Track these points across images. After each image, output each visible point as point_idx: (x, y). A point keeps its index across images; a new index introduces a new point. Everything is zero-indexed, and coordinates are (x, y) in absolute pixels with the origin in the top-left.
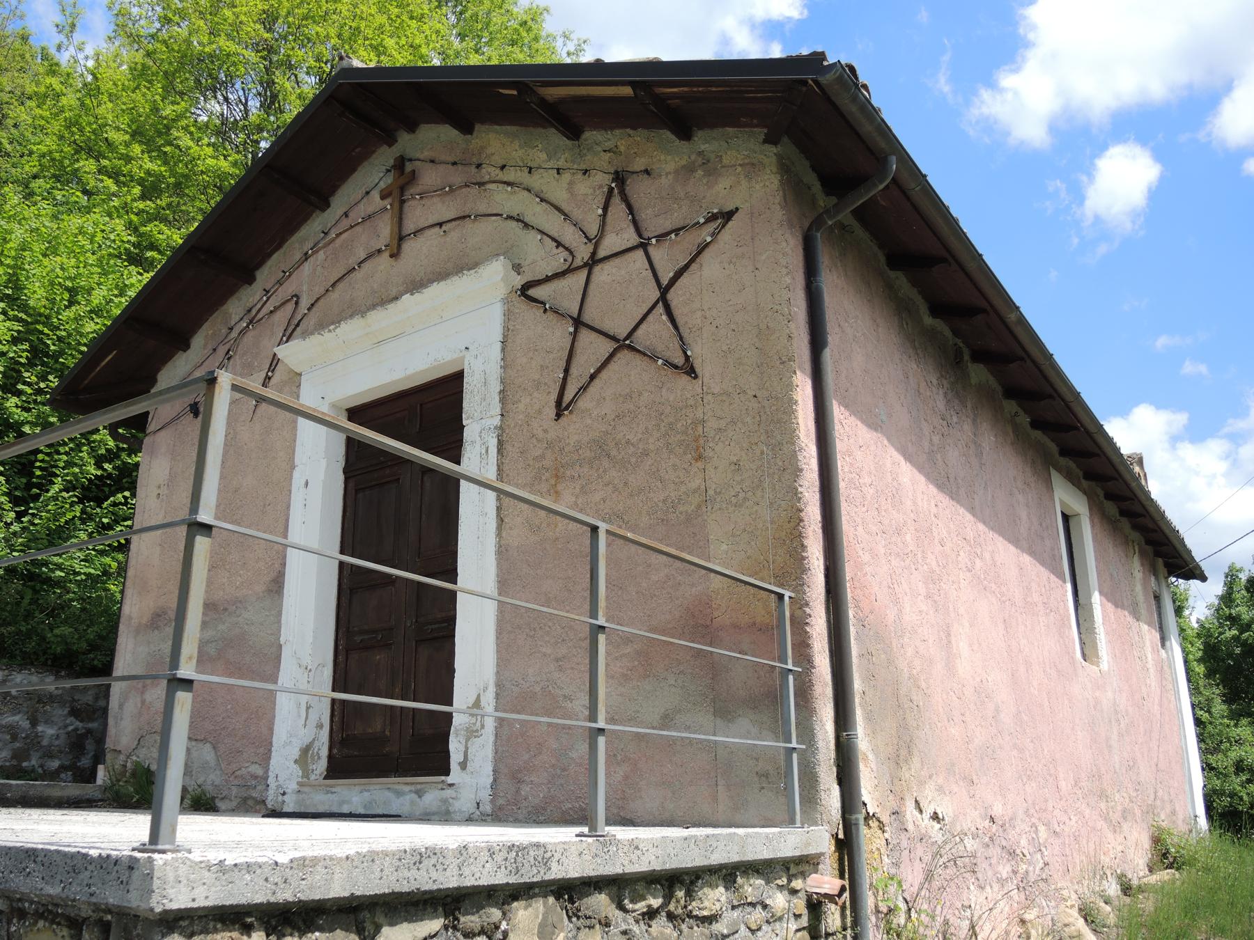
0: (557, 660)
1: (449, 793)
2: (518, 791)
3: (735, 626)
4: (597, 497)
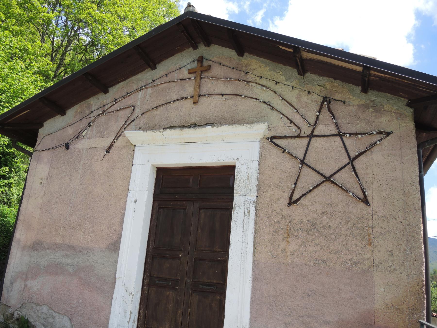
4: (311, 249)
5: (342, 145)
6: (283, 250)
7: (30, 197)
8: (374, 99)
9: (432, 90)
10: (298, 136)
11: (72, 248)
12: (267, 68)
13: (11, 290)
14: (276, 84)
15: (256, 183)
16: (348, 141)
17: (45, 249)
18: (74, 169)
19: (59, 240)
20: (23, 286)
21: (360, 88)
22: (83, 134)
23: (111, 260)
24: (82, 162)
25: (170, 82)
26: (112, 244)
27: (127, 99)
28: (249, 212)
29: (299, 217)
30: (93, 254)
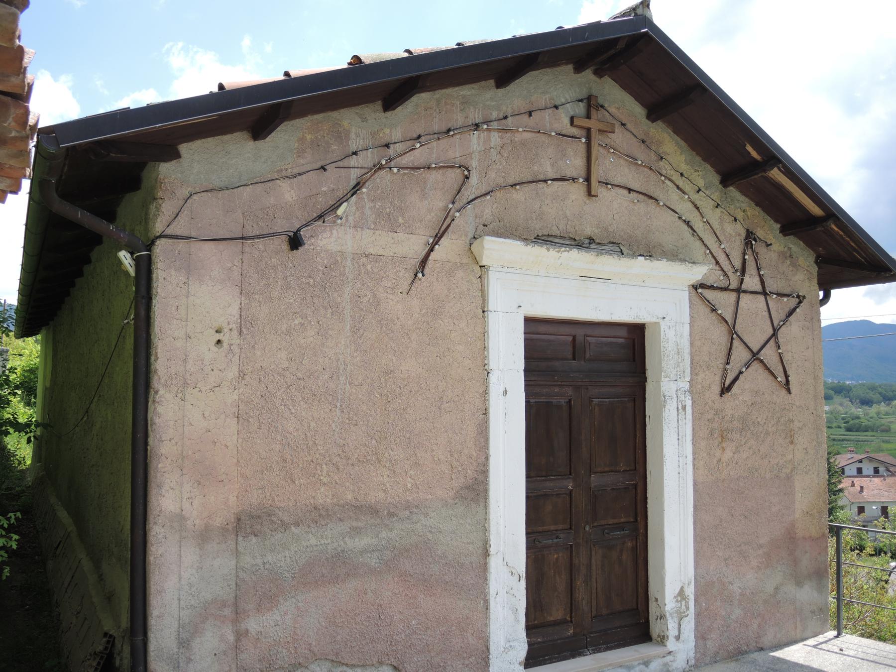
0: (726, 560)
1: (669, 658)
2: (706, 645)
3: (804, 538)
4: (744, 455)
5: (766, 308)
6: (719, 461)
7: (186, 384)
8: (791, 246)
9: (863, 258)
10: (726, 289)
11: (372, 510)
12: (683, 158)
13: (189, 660)
14: (698, 192)
15: (492, 318)
16: (773, 301)
17: (285, 526)
18: (326, 309)
19: (323, 497)
20: (231, 638)
21: (779, 226)
22: (340, 212)
23: (469, 521)
24: (347, 290)
25: (539, 132)
26: (467, 487)
27: (444, 142)
28: (684, 408)
29: (731, 412)
30: (426, 515)
